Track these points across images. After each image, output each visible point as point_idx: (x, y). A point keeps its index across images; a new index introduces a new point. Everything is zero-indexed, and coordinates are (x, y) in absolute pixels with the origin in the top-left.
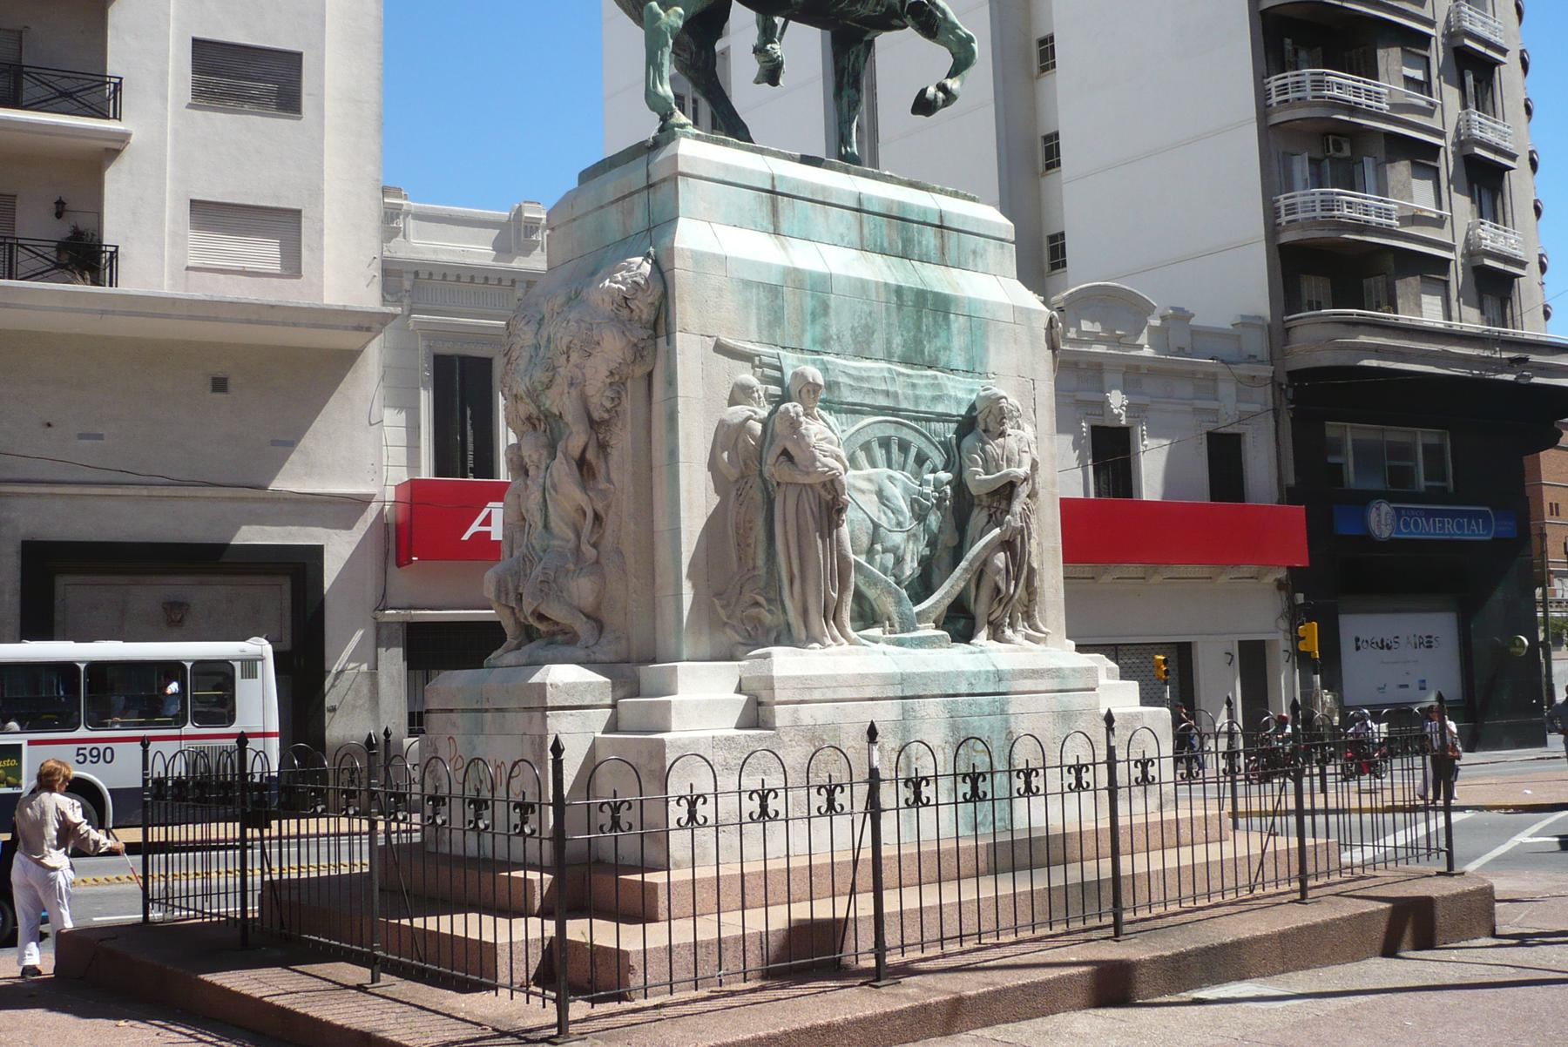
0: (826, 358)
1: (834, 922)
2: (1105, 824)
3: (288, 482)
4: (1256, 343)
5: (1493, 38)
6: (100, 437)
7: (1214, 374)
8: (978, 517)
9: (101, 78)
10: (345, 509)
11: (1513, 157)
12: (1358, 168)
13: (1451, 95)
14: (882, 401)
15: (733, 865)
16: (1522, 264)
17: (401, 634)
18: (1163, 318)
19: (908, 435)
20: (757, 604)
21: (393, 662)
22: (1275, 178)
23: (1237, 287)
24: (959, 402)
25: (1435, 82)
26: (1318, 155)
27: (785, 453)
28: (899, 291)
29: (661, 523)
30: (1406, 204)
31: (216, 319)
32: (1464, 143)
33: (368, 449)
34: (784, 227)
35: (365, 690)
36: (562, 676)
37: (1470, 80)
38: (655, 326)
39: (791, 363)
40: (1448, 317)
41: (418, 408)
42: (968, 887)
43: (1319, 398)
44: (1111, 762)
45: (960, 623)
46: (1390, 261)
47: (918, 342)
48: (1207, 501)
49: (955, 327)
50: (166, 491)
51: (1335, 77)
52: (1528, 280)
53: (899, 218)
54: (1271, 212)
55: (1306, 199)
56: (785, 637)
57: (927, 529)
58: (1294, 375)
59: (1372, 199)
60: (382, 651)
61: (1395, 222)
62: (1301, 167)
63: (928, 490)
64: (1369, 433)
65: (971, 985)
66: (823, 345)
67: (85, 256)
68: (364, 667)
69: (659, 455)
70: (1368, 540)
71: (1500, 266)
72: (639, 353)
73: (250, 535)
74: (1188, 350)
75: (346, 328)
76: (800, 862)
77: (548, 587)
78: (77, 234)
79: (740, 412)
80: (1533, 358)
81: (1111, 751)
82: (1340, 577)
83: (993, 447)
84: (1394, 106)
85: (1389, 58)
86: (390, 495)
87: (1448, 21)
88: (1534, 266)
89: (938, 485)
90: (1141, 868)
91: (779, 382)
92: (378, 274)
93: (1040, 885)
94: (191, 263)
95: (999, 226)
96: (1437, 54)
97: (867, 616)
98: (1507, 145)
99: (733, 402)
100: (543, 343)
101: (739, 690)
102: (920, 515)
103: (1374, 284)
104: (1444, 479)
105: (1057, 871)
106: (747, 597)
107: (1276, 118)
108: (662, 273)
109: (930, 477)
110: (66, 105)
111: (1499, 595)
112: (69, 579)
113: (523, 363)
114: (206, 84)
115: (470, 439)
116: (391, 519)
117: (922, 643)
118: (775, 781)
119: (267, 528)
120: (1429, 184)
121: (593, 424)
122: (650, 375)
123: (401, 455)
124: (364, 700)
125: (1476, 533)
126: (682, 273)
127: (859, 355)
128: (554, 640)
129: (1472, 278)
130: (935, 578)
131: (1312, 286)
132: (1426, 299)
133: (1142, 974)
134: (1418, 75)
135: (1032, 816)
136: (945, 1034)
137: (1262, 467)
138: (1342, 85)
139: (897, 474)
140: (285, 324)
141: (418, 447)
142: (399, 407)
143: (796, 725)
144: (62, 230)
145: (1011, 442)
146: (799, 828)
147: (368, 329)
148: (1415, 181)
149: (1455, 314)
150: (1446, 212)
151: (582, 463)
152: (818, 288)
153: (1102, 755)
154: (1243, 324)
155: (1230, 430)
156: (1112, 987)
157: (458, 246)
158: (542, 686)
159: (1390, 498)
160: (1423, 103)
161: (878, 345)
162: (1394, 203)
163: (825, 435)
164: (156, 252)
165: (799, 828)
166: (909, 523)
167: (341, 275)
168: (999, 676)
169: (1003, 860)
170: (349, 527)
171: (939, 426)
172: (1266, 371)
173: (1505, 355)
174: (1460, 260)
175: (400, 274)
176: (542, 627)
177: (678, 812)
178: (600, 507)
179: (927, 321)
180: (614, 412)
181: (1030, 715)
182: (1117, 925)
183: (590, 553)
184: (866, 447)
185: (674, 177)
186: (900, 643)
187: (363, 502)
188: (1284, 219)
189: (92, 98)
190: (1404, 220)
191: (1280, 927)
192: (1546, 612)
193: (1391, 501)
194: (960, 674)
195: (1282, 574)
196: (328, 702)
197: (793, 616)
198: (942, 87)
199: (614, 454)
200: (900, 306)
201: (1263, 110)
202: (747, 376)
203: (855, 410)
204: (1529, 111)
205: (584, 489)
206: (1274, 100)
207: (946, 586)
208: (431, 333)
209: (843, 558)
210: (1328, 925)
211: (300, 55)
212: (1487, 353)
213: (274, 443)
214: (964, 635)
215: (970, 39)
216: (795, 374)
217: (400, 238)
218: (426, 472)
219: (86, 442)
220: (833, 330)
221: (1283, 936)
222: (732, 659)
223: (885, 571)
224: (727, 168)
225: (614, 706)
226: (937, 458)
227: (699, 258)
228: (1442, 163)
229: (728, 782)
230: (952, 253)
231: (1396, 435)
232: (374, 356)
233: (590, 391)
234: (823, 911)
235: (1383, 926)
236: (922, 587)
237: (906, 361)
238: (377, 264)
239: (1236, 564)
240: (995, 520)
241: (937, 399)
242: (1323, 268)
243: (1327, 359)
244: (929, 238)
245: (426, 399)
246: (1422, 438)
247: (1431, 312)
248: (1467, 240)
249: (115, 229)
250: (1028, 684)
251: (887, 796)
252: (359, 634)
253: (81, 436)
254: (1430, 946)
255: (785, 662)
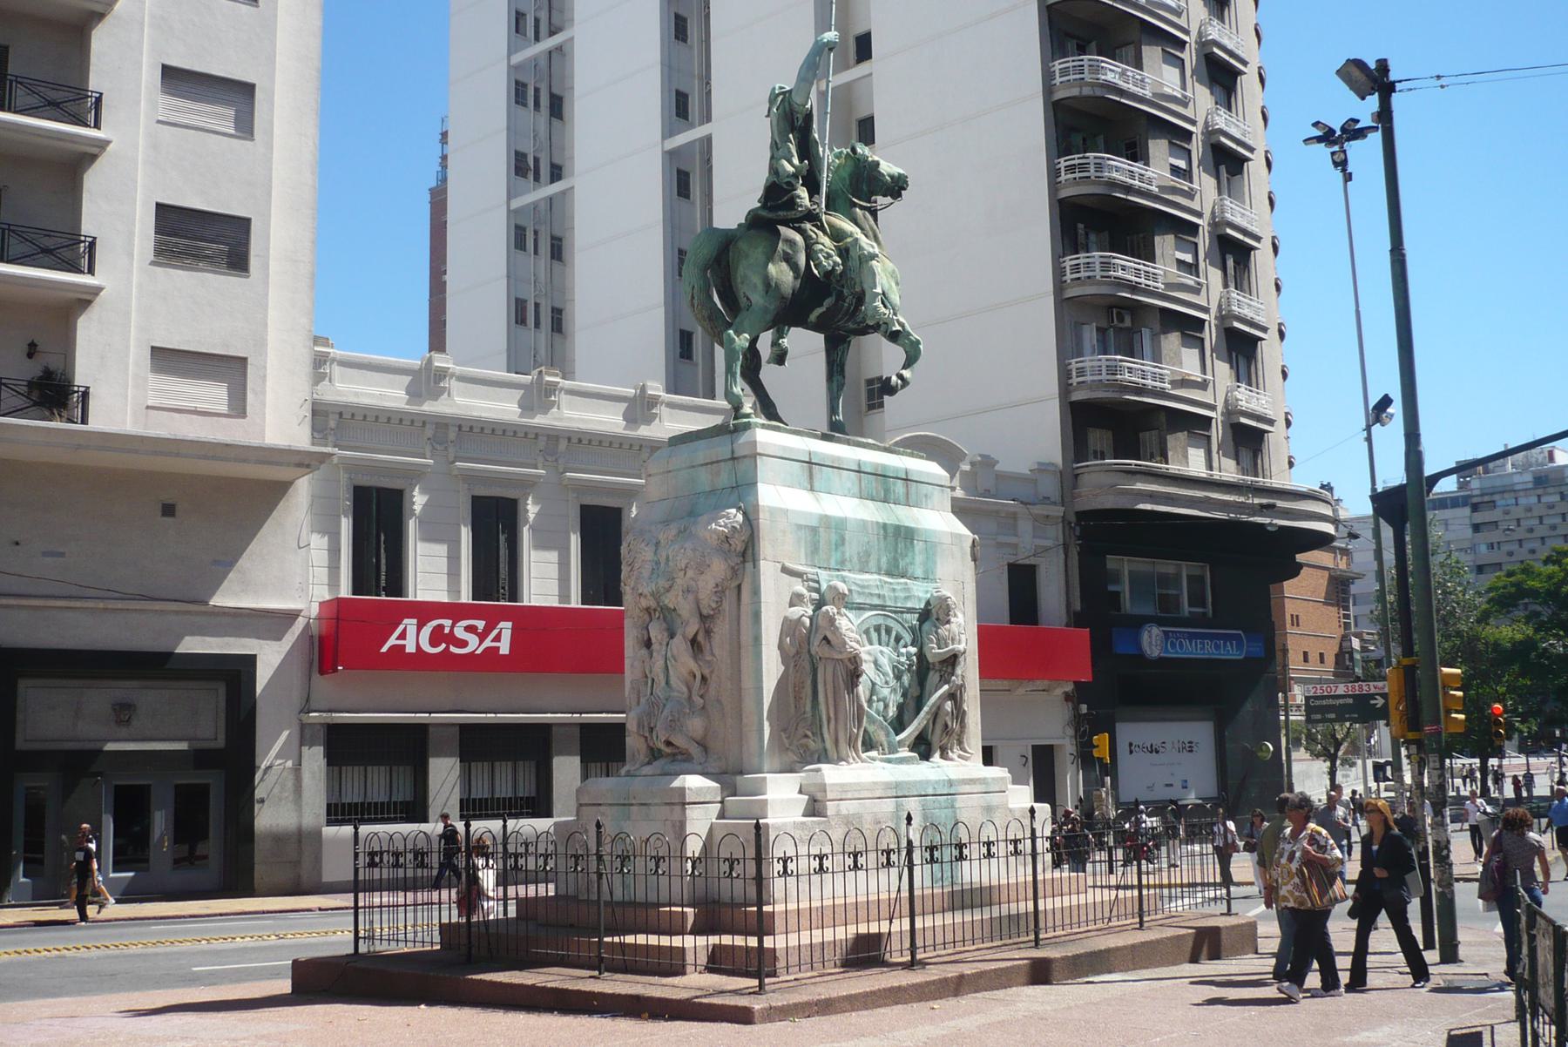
0: (845, 573)
1: (879, 935)
2: (1030, 878)
3: (220, 600)
4: (1050, 487)
5: (1251, 228)
6: (62, 555)
7: (1015, 514)
8: (933, 677)
9: (74, 237)
10: (273, 623)
11: (1265, 330)
12: (1137, 337)
13: (1215, 275)
14: (876, 601)
15: (812, 905)
16: (1271, 422)
17: (322, 734)
18: (972, 464)
19: (891, 623)
20: (806, 736)
21: (315, 758)
22: (1068, 346)
23: (1036, 437)
24: (920, 599)
25: (1202, 265)
26: (1104, 324)
27: (825, 638)
28: (885, 526)
29: (747, 683)
30: (1178, 370)
31: (178, 455)
32: (1225, 317)
33: (294, 570)
34: (817, 485)
35: (290, 784)
36: (693, 782)
37: (1230, 263)
38: (744, 554)
39: (826, 579)
40: (1210, 467)
41: (338, 534)
42: (939, 917)
43: (1103, 534)
44: (1033, 838)
45: (923, 748)
46: (1163, 417)
47: (895, 559)
48: (1007, 624)
49: (917, 549)
50: (120, 605)
51: (1121, 260)
52: (1276, 435)
53: (881, 475)
54: (1064, 373)
55: (1093, 363)
56: (823, 757)
57: (902, 686)
58: (1082, 516)
59: (1148, 366)
60: (305, 749)
61: (1167, 385)
62: (1090, 335)
63: (903, 659)
64: (1141, 565)
65: (968, 970)
66: (841, 565)
67: (55, 392)
68: (289, 764)
69: (746, 638)
70: (1141, 657)
71: (1253, 423)
72: (735, 572)
73: (193, 645)
74: (993, 492)
75: (289, 465)
76: (862, 899)
77: (674, 724)
78: (48, 374)
79: (796, 612)
80: (1280, 504)
81: (1033, 831)
82: (1120, 689)
83: (943, 631)
84: (1169, 286)
85: (1165, 244)
86: (315, 610)
87: (1213, 213)
88: (1281, 423)
89: (909, 656)
90: (1050, 906)
91: (817, 591)
92: (309, 414)
93: (986, 916)
94: (150, 403)
95: (940, 477)
96: (1203, 240)
97: (869, 745)
98: (1261, 319)
99: (792, 605)
100: (663, 560)
101: (800, 792)
102: (898, 677)
103: (1149, 438)
104: (1204, 605)
105: (986, 909)
106: (801, 732)
107: (1070, 293)
108: (751, 522)
109: (903, 650)
110: (47, 259)
111: (1248, 706)
112: (30, 682)
113: (646, 573)
114: (166, 244)
115: (383, 561)
116: (315, 630)
117: (902, 761)
118: (826, 850)
119: (208, 639)
120: (1196, 352)
121: (703, 618)
122: (739, 587)
123: (322, 574)
124: (289, 793)
125: (1231, 653)
126: (764, 521)
127: (862, 571)
128: (680, 760)
129: (1229, 431)
130: (906, 718)
131: (1098, 438)
132: (1191, 451)
133: (1056, 967)
134: (1188, 258)
135: (974, 873)
136: (956, 996)
137: (1053, 596)
138: (1126, 267)
139: (884, 649)
140: (236, 460)
141: (338, 568)
142: (323, 532)
143: (838, 815)
144: (32, 370)
145: (953, 627)
146: (839, 878)
147: (308, 466)
148: (1184, 350)
149: (1215, 464)
150: (1209, 377)
151: (694, 642)
152: (836, 527)
153: (1028, 835)
154: (1039, 470)
155: (1027, 562)
156: (1040, 973)
157: (376, 390)
158: (682, 790)
159: (1160, 622)
160: (1191, 283)
161: (872, 564)
162: (1167, 370)
163: (849, 624)
164: (123, 397)
165: (839, 878)
166: (893, 682)
167: (278, 419)
168: (951, 783)
169: (958, 903)
170: (279, 639)
171: (908, 616)
172: (1058, 511)
173: (1256, 501)
174: (1220, 419)
175: (326, 414)
176: (668, 750)
177: (779, 867)
178: (706, 672)
179: (901, 545)
180: (718, 610)
181: (969, 809)
182: (1037, 940)
183: (698, 701)
184: (867, 632)
185: (754, 456)
186: (889, 761)
187: (292, 616)
188: (1075, 380)
189: (66, 253)
190: (1174, 384)
191: (1130, 942)
192: (1287, 716)
193: (1160, 625)
194: (928, 782)
195: (1069, 687)
196: (258, 794)
197: (829, 744)
198: (900, 377)
199: (717, 639)
200: (885, 538)
201: (1059, 285)
202: (800, 588)
203: (860, 608)
204: (1278, 288)
205: (695, 658)
206: (1069, 277)
207: (916, 722)
208: (351, 467)
209: (860, 707)
210: (1158, 942)
211: (249, 220)
212: (1241, 499)
213: (216, 562)
214: (926, 756)
215: (918, 342)
216: (830, 587)
217: (326, 382)
218: (345, 591)
219: (48, 560)
220: (847, 555)
221: (1133, 946)
222: (791, 771)
223: (878, 712)
224: (784, 448)
225: (722, 802)
226: (908, 638)
227: (773, 511)
228: (1206, 335)
229: (803, 850)
230: (913, 498)
231: (1167, 567)
232: (303, 489)
233: (701, 596)
234: (874, 929)
235: (1190, 944)
236: (899, 725)
237: (889, 574)
238: (308, 406)
239: (1031, 679)
240: (945, 679)
241: (907, 598)
242: (1112, 424)
243: (1109, 502)
244: (899, 487)
245: (346, 526)
246: (1186, 569)
247: (1194, 463)
248: (1226, 401)
249: (83, 373)
250: (967, 788)
251: (917, 859)
252: (286, 733)
253: (45, 554)
254: (1218, 958)
255: (831, 774)
